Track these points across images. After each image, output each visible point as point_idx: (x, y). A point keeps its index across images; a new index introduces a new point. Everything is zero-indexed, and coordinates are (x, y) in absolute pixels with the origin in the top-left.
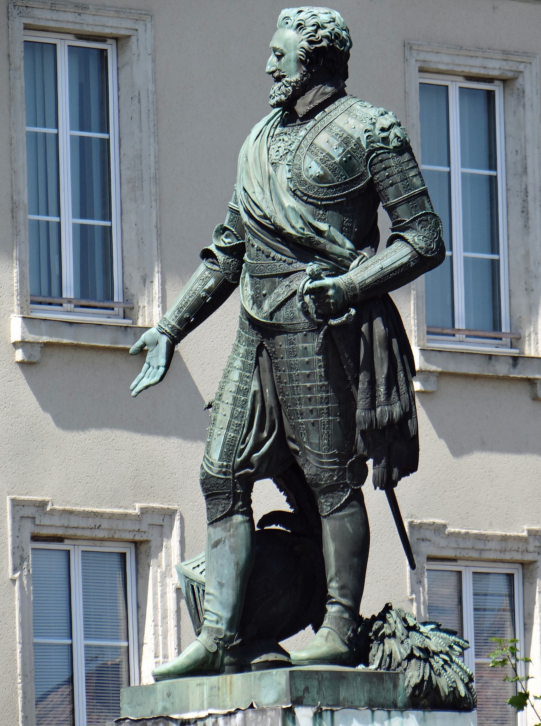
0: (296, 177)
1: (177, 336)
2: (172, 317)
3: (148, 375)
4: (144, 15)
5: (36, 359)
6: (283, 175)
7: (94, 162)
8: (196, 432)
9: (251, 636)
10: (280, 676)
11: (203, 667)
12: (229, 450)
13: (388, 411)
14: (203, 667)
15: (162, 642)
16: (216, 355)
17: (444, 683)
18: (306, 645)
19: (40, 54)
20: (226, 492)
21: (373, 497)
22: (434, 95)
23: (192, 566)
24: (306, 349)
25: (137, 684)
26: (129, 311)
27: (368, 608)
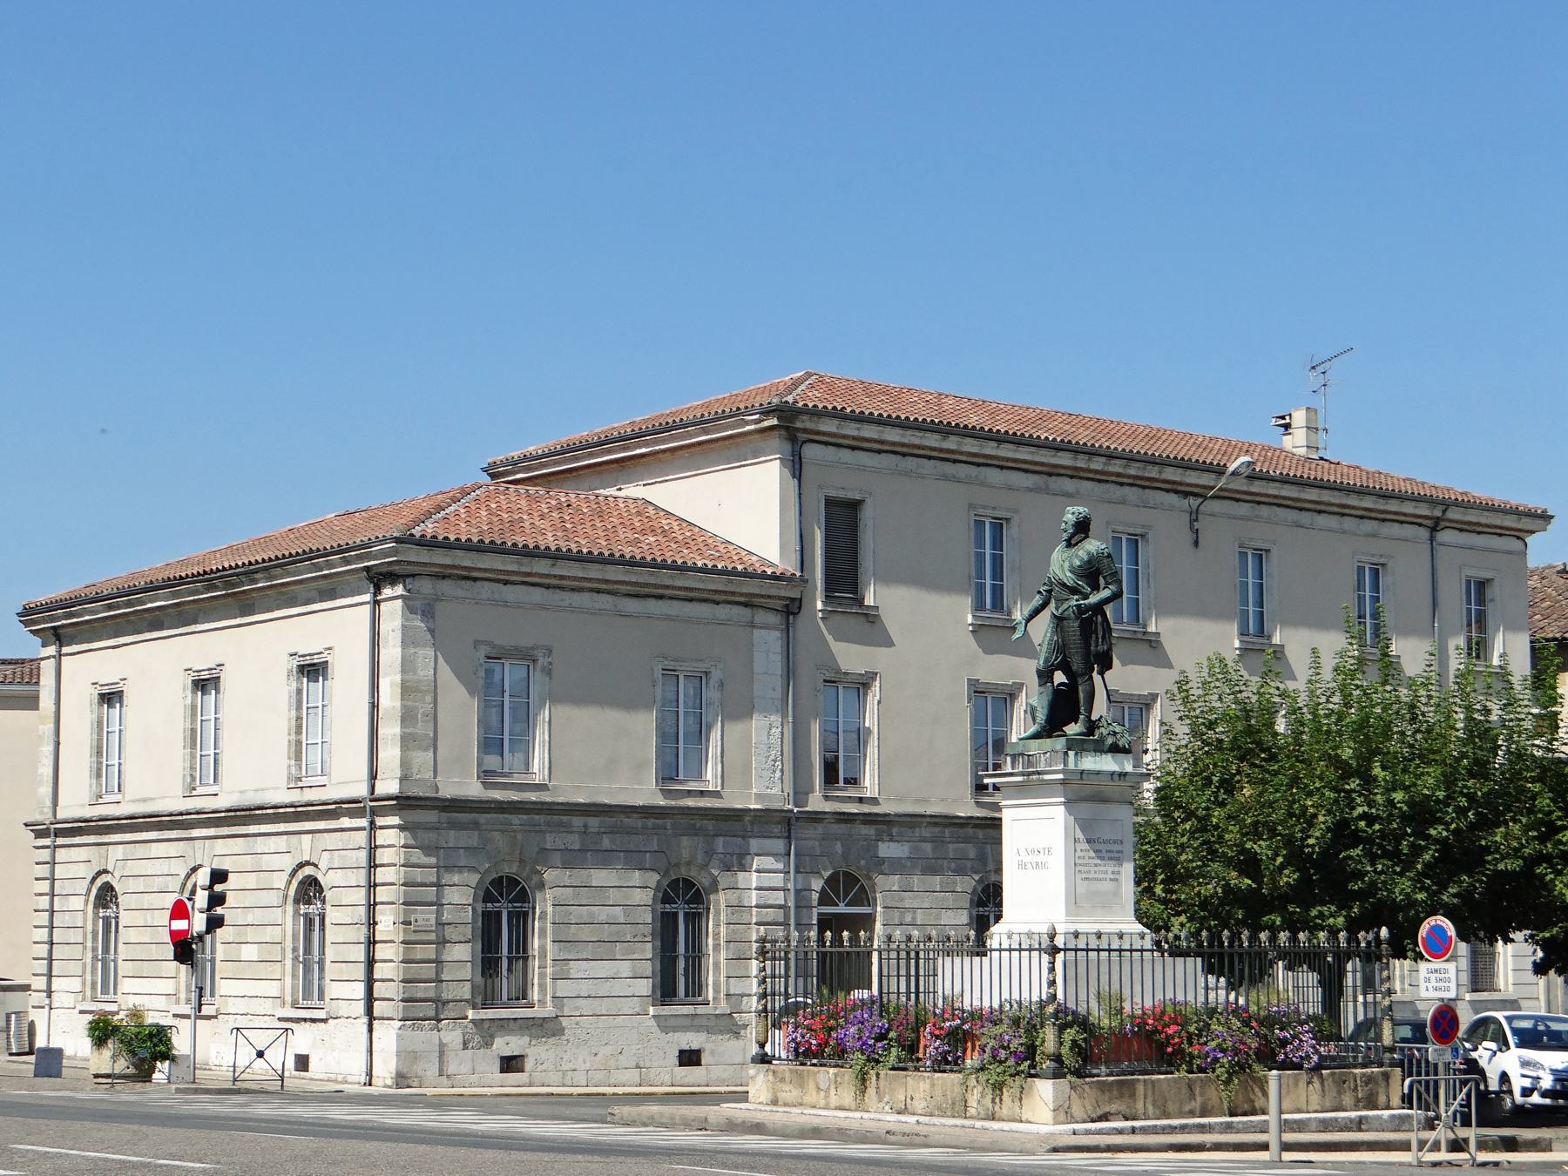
0: (1071, 565)
1: (1028, 620)
2: (1026, 613)
3: (1018, 635)
4: (1016, 511)
5: (977, 630)
6: (1067, 564)
7: (998, 562)
8: (1035, 656)
9: (1052, 727)
10: (1063, 740)
11: (1036, 736)
12: (1047, 660)
13: (1102, 648)
14: (1036, 736)
15: (1019, 728)
16: (1041, 631)
17: (1120, 744)
18: (1073, 729)
19: (980, 524)
20: (1045, 676)
21: (1096, 677)
22: (1117, 541)
23: (1030, 703)
24: (1074, 626)
25: (753, 849)
26: (1009, 614)
27: (1094, 717)
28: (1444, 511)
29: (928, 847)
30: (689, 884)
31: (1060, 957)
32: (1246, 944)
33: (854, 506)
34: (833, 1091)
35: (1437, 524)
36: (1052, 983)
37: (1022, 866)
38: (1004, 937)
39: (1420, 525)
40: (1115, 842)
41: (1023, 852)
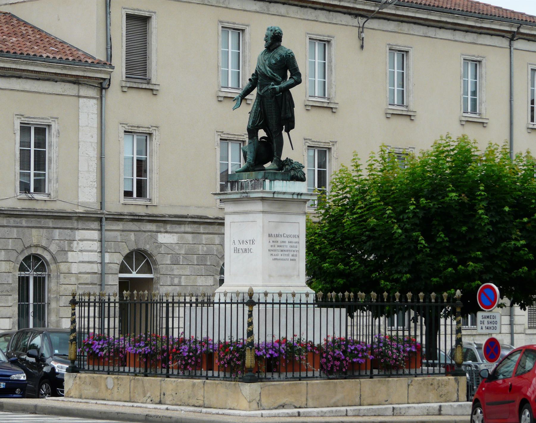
6: (267, 62)
10: (262, 172)
14: (246, 170)
21: (284, 134)
25: (77, 238)
27: (283, 158)
28: (518, 28)
29: (189, 237)
30: (37, 258)
31: (255, 308)
32: (421, 301)
33: (145, 20)
34: (116, 390)
35: (513, 36)
36: (250, 324)
37: (236, 250)
38: (290, 296)
39: (503, 37)
40: (294, 236)
41: (237, 242)
